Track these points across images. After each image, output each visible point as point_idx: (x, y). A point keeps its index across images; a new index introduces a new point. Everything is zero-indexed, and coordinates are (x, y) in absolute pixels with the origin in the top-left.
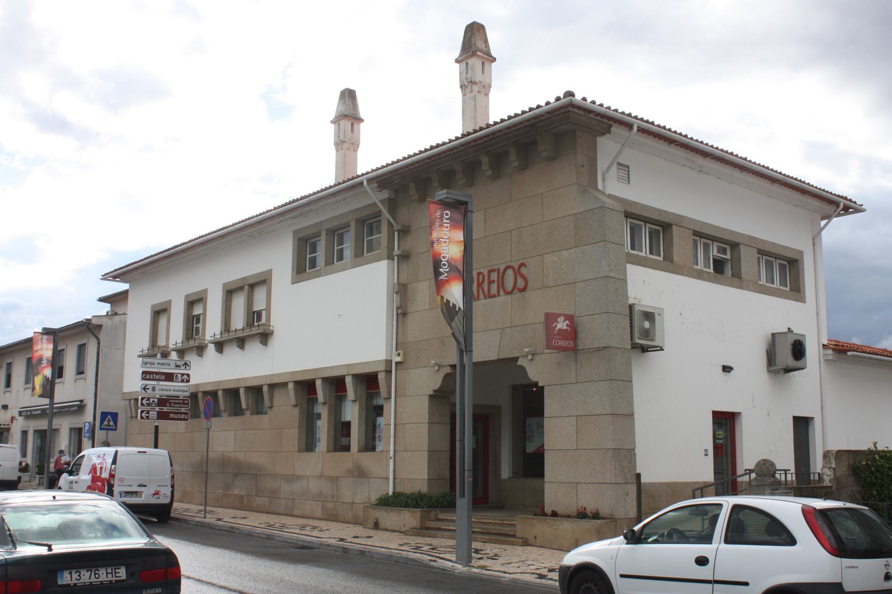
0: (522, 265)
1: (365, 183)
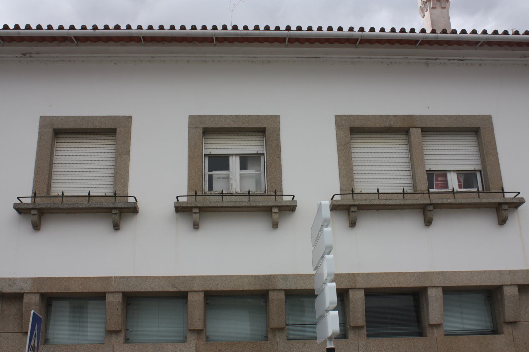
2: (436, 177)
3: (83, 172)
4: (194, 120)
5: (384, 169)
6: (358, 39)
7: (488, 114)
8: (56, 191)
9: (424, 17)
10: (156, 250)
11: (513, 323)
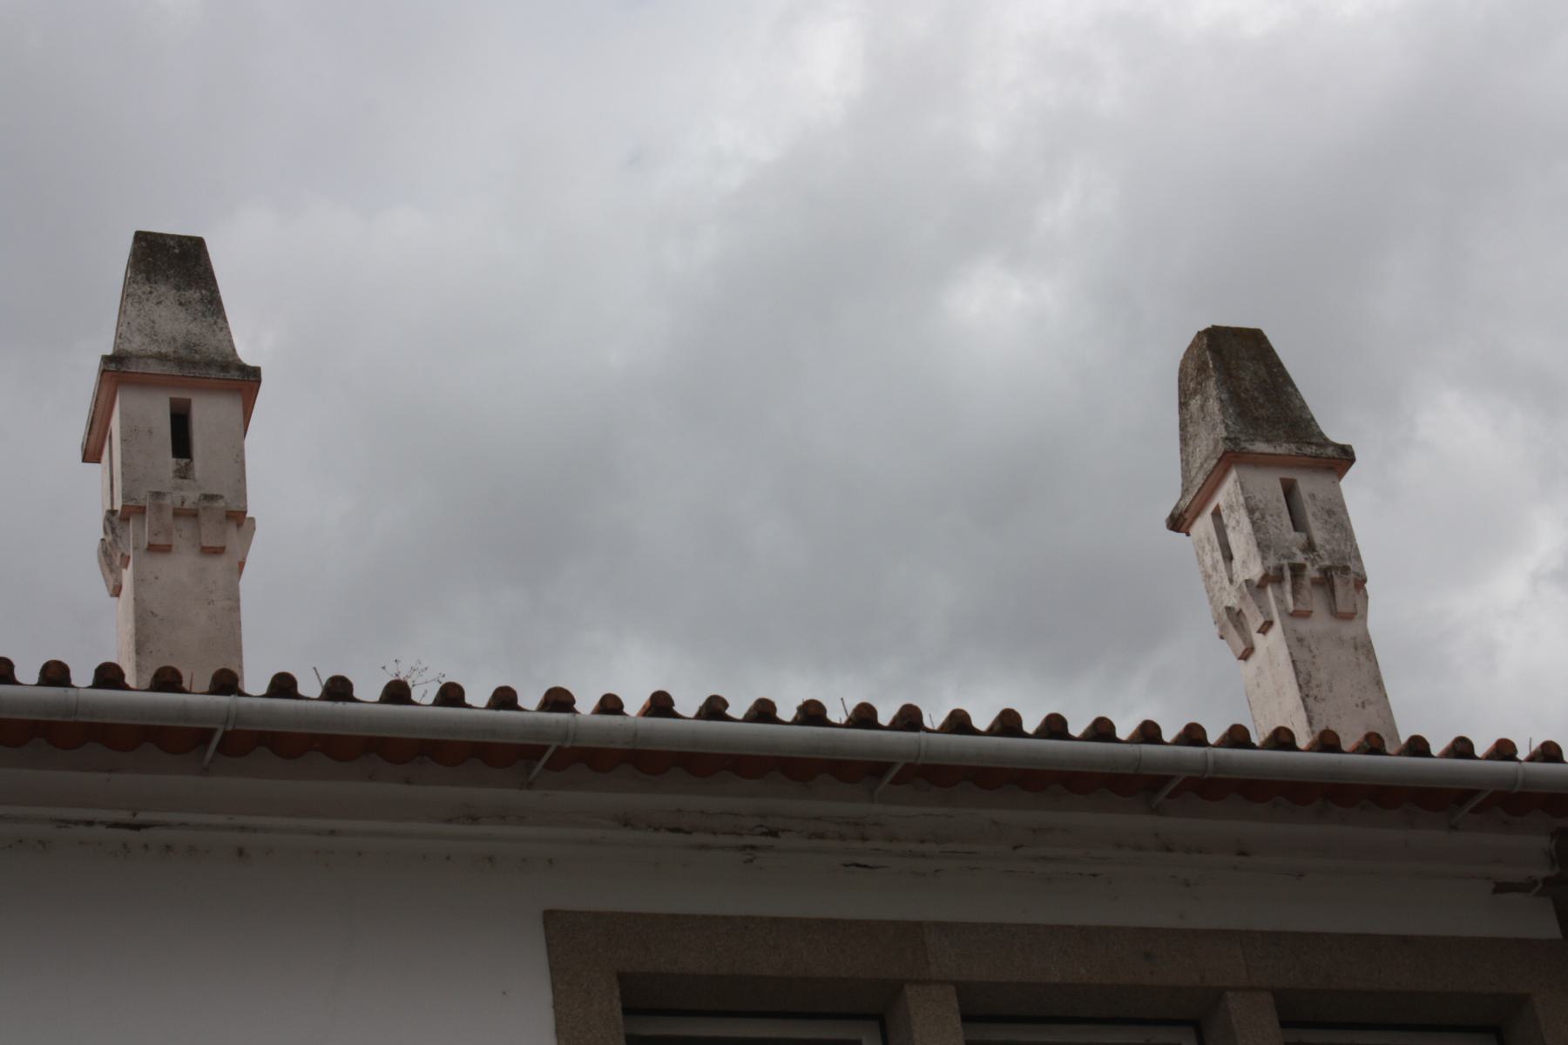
6: (212, 732)
9: (1246, 655)
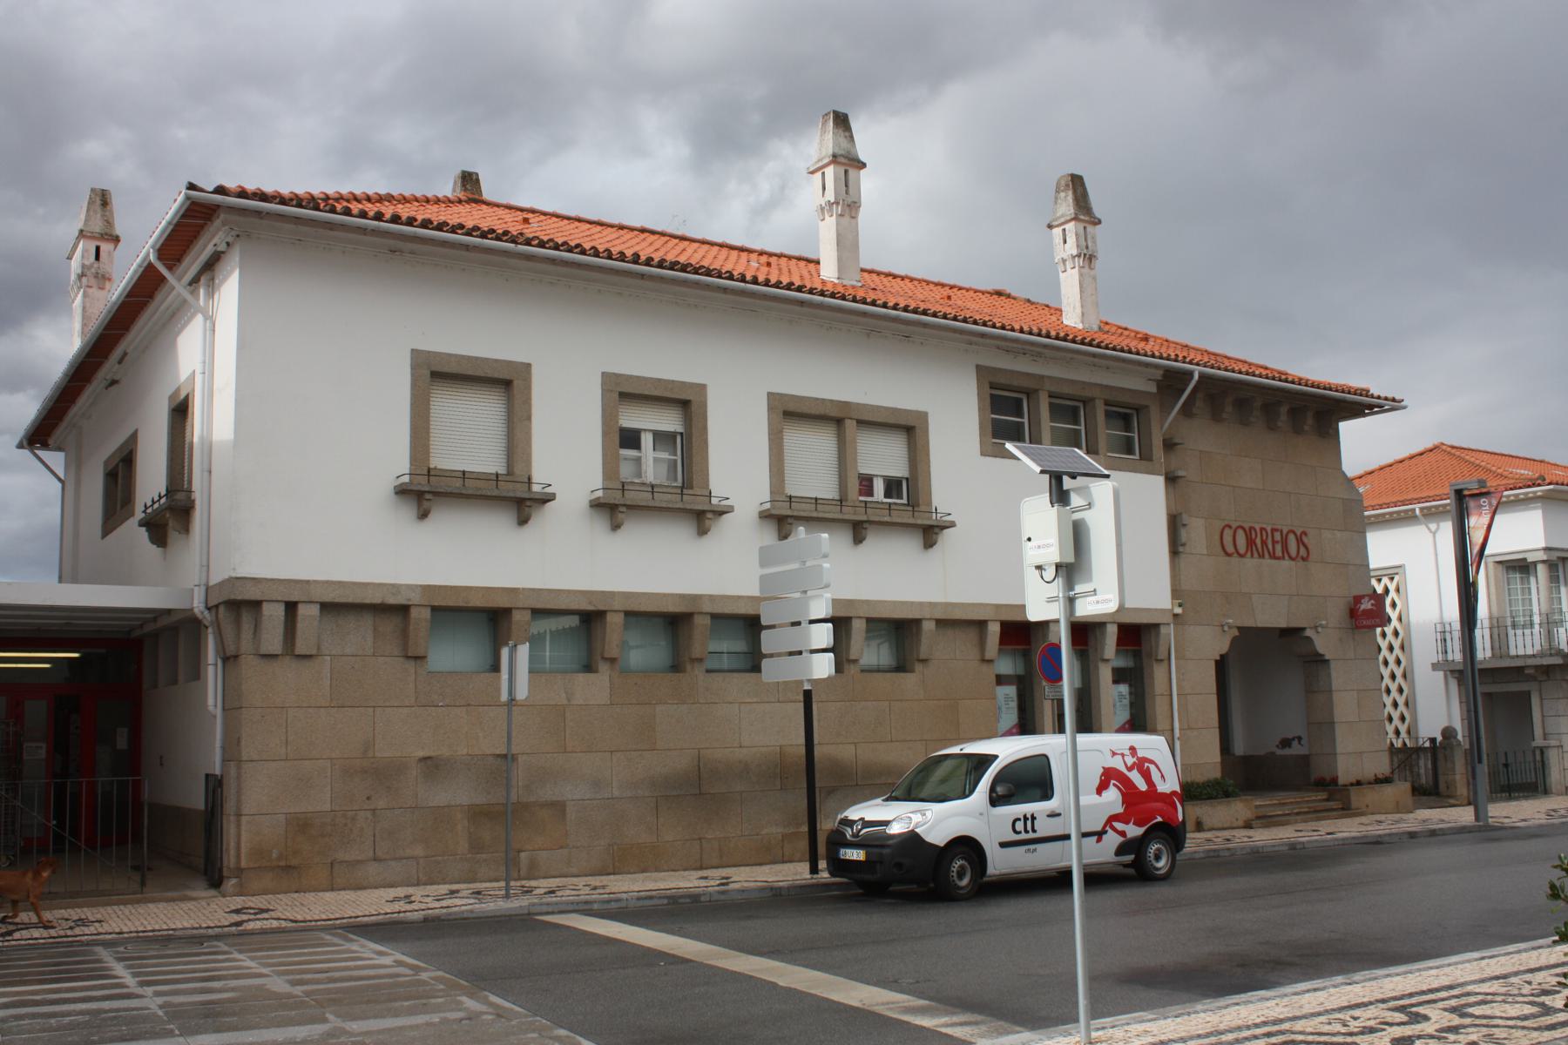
0: (1304, 533)
1: (1196, 376)
2: (866, 483)
3: (469, 437)
4: (609, 380)
5: (813, 468)
7: (921, 409)
8: (1216, 773)
10: (564, 556)
11: (924, 661)
